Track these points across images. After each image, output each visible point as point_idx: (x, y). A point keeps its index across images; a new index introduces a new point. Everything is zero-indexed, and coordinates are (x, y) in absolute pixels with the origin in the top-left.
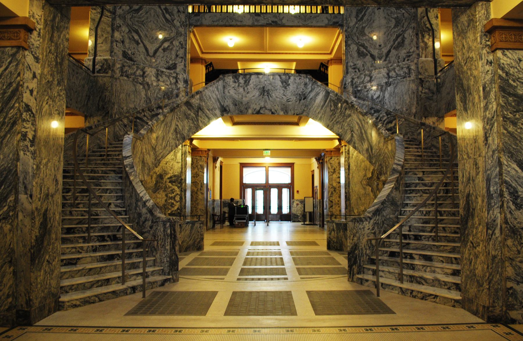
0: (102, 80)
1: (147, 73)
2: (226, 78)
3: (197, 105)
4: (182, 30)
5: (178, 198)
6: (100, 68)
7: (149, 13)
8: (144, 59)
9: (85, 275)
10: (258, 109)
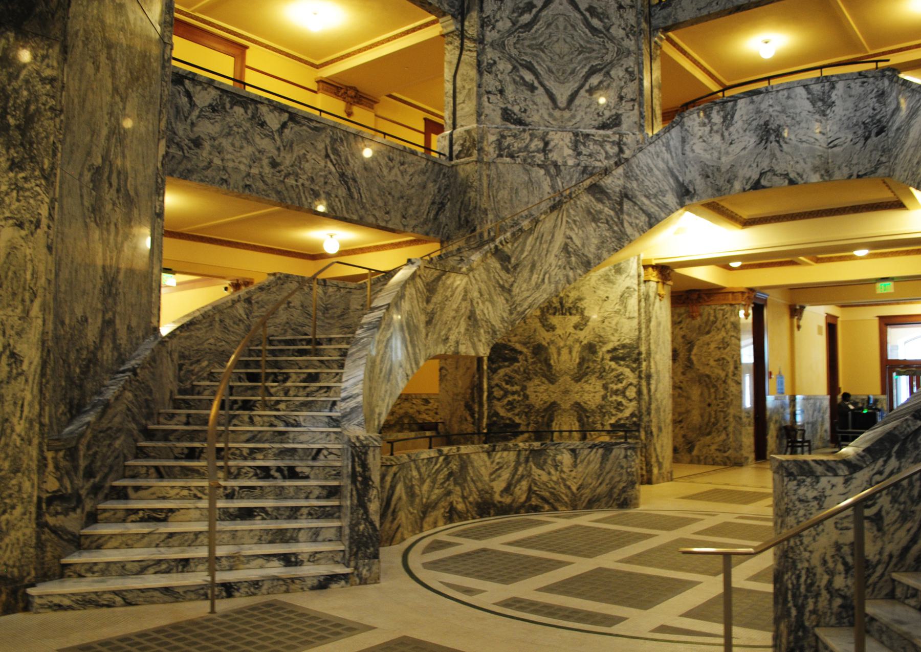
0: (463, 170)
1: (552, 144)
2: (685, 120)
3: (617, 189)
4: (630, 44)
5: (632, 393)
6: (460, 148)
7: (553, 26)
8: (546, 117)
9: (157, 546)
10: (755, 177)
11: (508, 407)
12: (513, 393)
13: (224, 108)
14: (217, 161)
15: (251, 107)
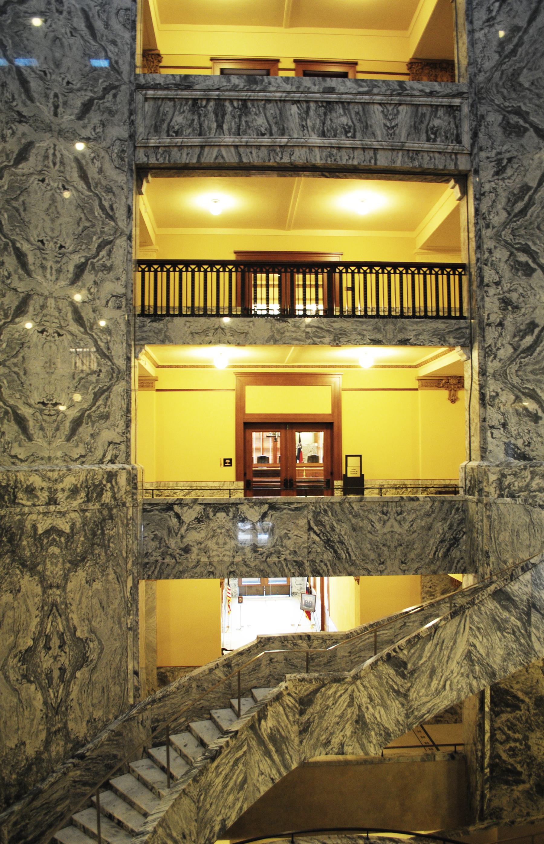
3: (525, 598)
11: (511, 753)
12: (515, 740)
13: (208, 517)
14: (204, 559)
15: (232, 510)
